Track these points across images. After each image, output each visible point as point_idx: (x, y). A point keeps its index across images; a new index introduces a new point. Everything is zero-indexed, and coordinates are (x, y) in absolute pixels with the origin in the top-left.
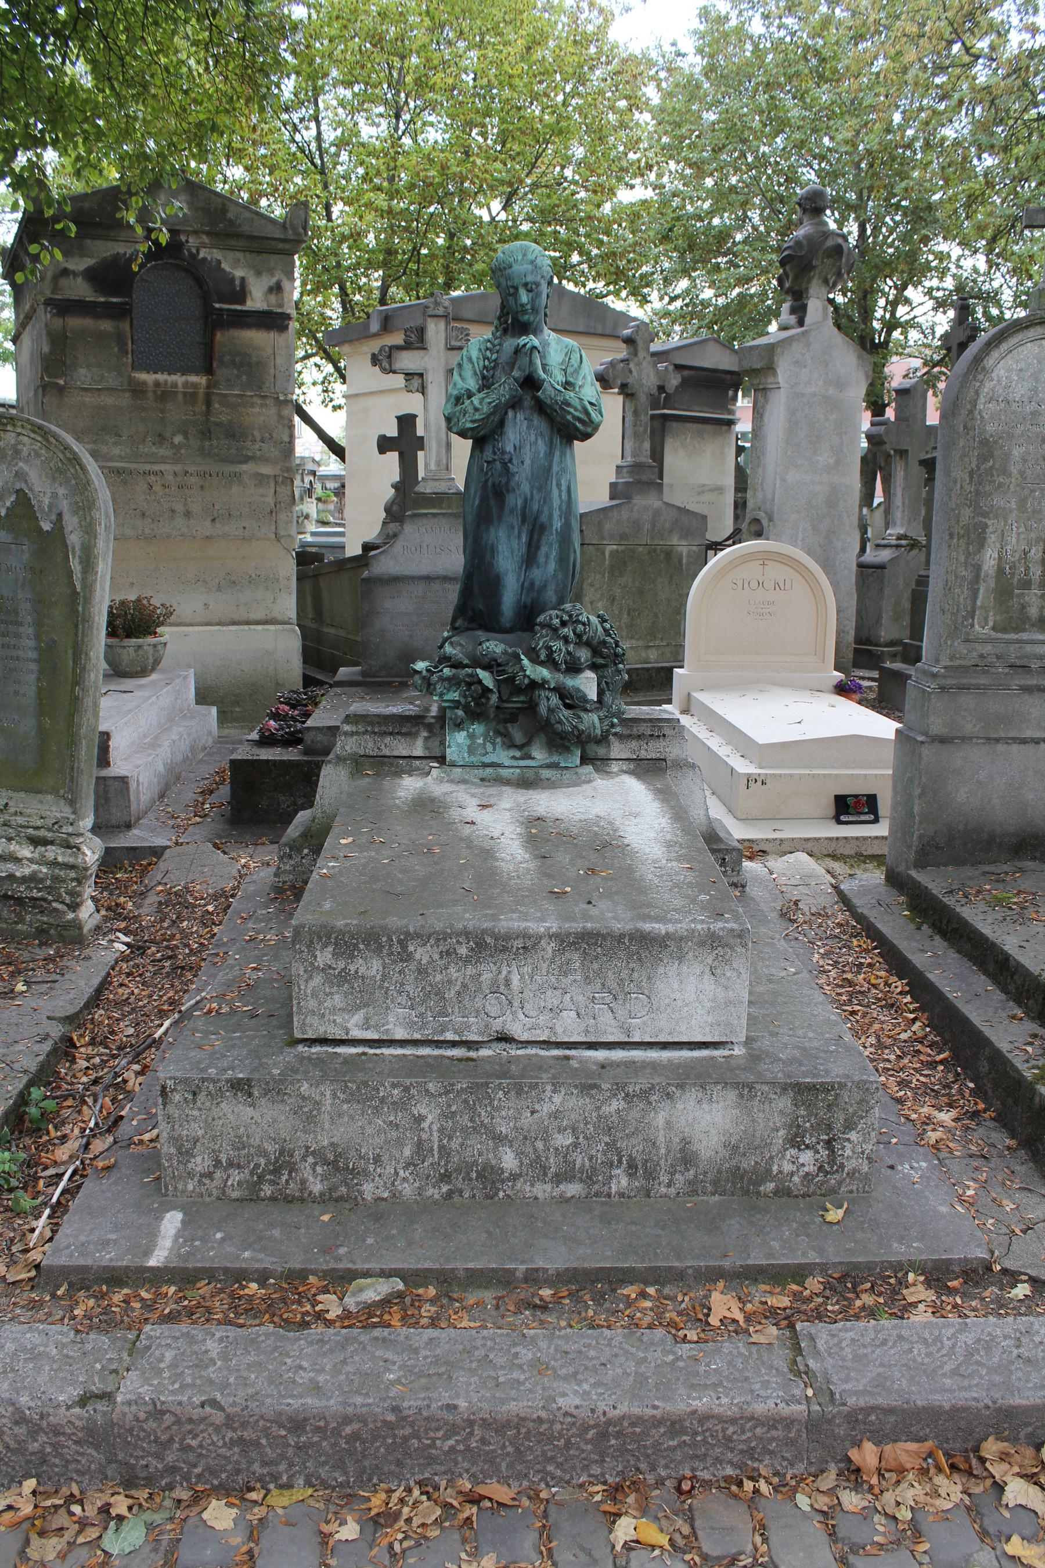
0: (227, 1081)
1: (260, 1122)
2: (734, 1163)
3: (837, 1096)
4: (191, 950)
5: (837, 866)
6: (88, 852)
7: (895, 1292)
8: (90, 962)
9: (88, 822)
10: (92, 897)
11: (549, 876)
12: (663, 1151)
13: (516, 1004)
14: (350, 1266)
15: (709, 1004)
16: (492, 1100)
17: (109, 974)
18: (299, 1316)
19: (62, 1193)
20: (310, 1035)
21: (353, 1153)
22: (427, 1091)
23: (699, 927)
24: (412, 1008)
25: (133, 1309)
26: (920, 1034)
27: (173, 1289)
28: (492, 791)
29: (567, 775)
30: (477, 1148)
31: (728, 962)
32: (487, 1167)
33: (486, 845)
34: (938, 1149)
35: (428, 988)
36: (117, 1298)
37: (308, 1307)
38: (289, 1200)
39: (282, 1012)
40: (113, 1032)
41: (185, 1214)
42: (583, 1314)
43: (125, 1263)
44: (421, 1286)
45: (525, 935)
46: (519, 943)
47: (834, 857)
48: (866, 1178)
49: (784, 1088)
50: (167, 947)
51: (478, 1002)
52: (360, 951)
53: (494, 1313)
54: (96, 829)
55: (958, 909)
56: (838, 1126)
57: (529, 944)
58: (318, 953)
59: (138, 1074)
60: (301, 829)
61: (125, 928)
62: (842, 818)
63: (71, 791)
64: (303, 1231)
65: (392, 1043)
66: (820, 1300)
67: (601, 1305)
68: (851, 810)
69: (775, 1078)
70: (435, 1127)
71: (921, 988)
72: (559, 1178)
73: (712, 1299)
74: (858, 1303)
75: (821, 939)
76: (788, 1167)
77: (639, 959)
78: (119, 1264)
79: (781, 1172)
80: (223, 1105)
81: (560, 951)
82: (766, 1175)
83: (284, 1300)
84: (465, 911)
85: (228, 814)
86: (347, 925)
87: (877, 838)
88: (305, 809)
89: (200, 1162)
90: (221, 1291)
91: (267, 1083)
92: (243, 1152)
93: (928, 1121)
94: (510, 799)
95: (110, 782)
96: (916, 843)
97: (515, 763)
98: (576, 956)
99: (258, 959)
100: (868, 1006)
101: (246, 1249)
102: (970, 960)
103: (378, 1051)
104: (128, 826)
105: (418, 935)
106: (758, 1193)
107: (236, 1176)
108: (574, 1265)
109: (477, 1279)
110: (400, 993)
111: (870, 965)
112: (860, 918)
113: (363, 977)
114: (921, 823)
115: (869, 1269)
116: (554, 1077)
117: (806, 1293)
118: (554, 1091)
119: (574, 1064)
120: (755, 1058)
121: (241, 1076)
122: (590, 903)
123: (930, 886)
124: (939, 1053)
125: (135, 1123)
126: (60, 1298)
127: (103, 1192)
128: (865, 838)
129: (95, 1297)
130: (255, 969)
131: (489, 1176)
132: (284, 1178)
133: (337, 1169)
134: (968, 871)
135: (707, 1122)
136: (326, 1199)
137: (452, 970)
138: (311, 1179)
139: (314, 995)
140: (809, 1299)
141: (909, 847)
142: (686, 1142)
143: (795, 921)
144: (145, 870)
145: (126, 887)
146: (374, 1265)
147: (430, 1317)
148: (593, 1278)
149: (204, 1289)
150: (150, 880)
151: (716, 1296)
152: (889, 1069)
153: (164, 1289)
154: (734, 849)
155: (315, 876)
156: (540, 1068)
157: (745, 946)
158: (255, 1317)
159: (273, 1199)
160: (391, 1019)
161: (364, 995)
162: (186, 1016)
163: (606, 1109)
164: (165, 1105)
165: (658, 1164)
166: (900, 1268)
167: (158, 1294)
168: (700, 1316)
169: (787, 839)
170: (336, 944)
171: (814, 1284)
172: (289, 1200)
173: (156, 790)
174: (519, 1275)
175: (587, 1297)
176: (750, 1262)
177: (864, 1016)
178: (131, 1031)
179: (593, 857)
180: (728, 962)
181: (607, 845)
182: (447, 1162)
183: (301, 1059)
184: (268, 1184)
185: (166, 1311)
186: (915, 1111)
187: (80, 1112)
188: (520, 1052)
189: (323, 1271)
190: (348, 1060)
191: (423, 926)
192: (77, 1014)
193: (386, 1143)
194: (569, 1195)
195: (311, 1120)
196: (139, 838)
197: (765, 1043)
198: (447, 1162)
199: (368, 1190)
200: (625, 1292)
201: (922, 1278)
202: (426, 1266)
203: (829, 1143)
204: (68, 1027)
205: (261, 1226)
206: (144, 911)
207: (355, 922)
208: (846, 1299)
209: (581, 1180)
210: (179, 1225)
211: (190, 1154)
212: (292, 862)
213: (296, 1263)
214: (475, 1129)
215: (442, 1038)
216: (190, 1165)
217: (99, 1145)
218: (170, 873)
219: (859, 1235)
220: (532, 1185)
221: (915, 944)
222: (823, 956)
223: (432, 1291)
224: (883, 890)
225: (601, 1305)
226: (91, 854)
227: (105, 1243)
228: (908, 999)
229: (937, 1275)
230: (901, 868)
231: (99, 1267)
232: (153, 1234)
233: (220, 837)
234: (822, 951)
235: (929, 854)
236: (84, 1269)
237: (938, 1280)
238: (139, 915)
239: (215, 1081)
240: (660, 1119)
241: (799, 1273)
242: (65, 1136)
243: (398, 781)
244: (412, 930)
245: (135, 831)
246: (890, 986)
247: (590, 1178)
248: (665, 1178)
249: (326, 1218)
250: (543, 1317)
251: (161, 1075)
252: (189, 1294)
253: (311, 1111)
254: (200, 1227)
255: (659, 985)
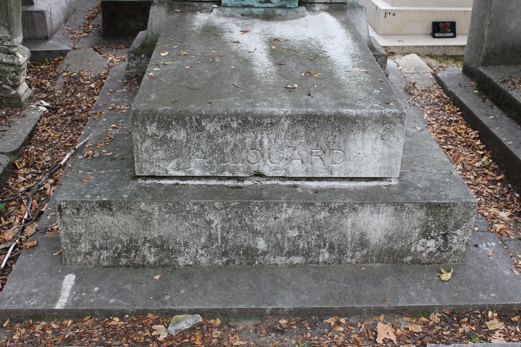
0: (97, 202)
1: (117, 225)
2: (389, 246)
3: (451, 210)
4: (82, 110)
5: (433, 62)
6: (20, 56)
7: (481, 323)
8: (26, 118)
9: (19, 39)
10: (26, 79)
11: (284, 77)
12: (349, 239)
13: (266, 156)
14: (171, 307)
15: (379, 157)
16: (252, 212)
17: (36, 125)
18: (143, 338)
19: (9, 259)
20: (145, 174)
21: (172, 241)
22: (214, 207)
23: (376, 111)
24: (205, 158)
25: (48, 335)
26: (487, 163)
27: (70, 322)
28: (249, 22)
29: (291, 12)
30: (243, 238)
31: (392, 132)
32: (249, 248)
33: (246, 57)
34: (501, 235)
35: (214, 147)
36: (38, 328)
37: (148, 333)
38: (136, 267)
39: (129, 156)
40: (39, 160)
41: (77, 276)
42: (305, 336)
43: (42, 307)
44: (212, 318)
45: (271, 116)
46: (268, 121)
47: (431, 56)
48: (464, 255)
49: (422, 206)
50: (69, 108)
51: (244, 155)
52: (173, 125)
53: (254, 335)
54: (25, 42)
55: (510, 92)
56: (451, 226)
57: (274, 122)
58: (148, 127)
59: (52, 185)
60: (140, 43)
61: (46, 98)
62: (436, 35)
63: (7, 21)
64: (144, 285)
65: (193, 178)
66: (439, 328)
67: (315, 329)
68: (441, 30)
69: (416, 200)
70: (219, 227)
71: (486, 136)
72: (290, 254)
73: (378, 327)
74: (461, 330)
75: (428, 105)
76: (420, 248)
77: (339, 130)
78: (39, 308)
79: (416, 251)
80: (95, 216)
81: (293, 125)
82: (408, 252)
83: (134, 328)
84: (236, 100)
85: (102, 31)
86: (165, 110)
87: (455, 46)
88: (142, 30)
89: (84, 247)
90: (98, 323)
91: (120, 203)
92: (108, 241)
93: (495, 217)
94: (259, 27)
95: (35, 14)
96: (484, 52)
97: (261, 5)
98: (302, 128)
99: (116, 122)
100: (456, 146)
101: (112, 298)
102: (516, 121)
103: (185, 182)
104: (47, 39)
105: (208, 116)
106: (402, 262)
107: (105, 254)
108: (299, 306)
109: (244, 314)
110: (197, 149)
111: (456, 121)
112: (449, 94)
113: (175, 141)
114: (488, 41)
115: (466, 309)
116: (288, 199)
117: (431, 323)
118: (288, 207)
119: (299, 190)
120: (404, 186)
121: (105, 199)
122: (309, 95)
123: (492, 77)
124: (498, 175)
125: (49, 217)
126: (6, 328)
127: (30, 262)
128: (448, 46)
129: (26, 327)
130: (114, 128)
131: (250, 253)
132: (133, 255)
133: (163, 250)
134: (513, 69)
135: (376, 224)
136: (158, 266)
137: (228, 136)
138: (148, 255)
139: (147, 151)
140: (433, 327)
141: (480, 54)
142: (363, 234)
143: (413, 94)
144: (56, 64)
145: (46, 73)
146: (185, 307)
147: (218, 338)
148: (310, 313)
149: (88, 321)
150: (60, 70)
151: (380, 326)
152: (470, 185)
153: (65, 322)
154: (383, 55)
155: (146, 77)
156: (280, 193)
157: (402, 123)
158: (117, 339)
159: (127, 266)
160: (192, 164)
161: (176, 151)
162: (78, 151)
163: (318, 217)
164: (61, 216)
165: (346, 247)
166: (484, 309)
167: (61, 325)
168: (371, 337)
169: (406, 47)
170: (158, 122)
171: (435, 318)
172: (136, 267)
173: (62, 17)
174: (268, 311)
175: (306, 324)
176: (399, 305)
177: (454, 151)
178: (49, 158)
179: (309, 64)
180: (392, 132)
181: (316, 56)
182: (226, 245)
183: (140, 188)
184: (124, 259)
185: (67, 336)
186: (487, 211)
187: (19, 209)
188: (268, 183)
189: (156, 310)
190: (168, 188)
191: (210, 111)
192: (18, 150)
193: (193, 238)
194: (295, 263)
195: (147, 223)
196: (53, 45)
197: (409, 177)
198: (226, 245)
199: (181, 260)
200: (328, 321)
201: (496, 315)
202: (215, 307)
203: (444, 236)
204: (12, 158)
205: (120, 283)
206: (57, 87)
207: (169, 108)
208: (453, 327)
209: (302, 255)
210: (73, 283)
211: (78, 242)
212: (136, 62)
213: (140, 307)
214: (242, 227)
215: (223, 175)
216: (78, 249)
217: (30, 230)
218: (71, 66)
219: (460, 289)
220: (275, 258)
221: (482, 111)
222: (430, 115)
223: (218, 322)
224: (462, 77)
225: (315, 329)
226: (23, 57)
227: (31, 295)
228: (479, 142)
229: (505, 314)
230: (474, 66)
231: (27, 310)
232: (58, 289)
233: (97, 44)
234: (429, 112)
235: (489, 59)
236: (18, 311)
237: (505, 316)
238: (54, 90)
239: (89, 203)
240: (349, 222)
241: (426, 311)
242: (11, 224)
243: (194, 16)
244: (204, 113)
245: (51, 42)
246: (468, 134)
247: (307, 254)
248: (350, 254)
249: (157, 277)
250: (282, 337)
251: (58, 199)
252: (79, 325)
253: (147, 219)
254: (85, 284)
255: (351, 145)
